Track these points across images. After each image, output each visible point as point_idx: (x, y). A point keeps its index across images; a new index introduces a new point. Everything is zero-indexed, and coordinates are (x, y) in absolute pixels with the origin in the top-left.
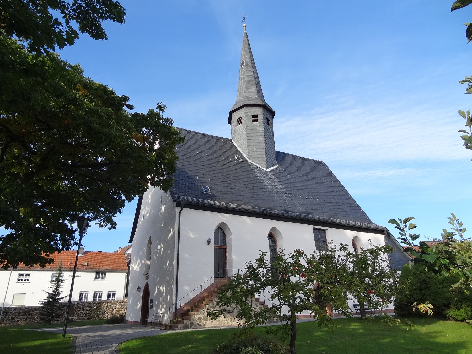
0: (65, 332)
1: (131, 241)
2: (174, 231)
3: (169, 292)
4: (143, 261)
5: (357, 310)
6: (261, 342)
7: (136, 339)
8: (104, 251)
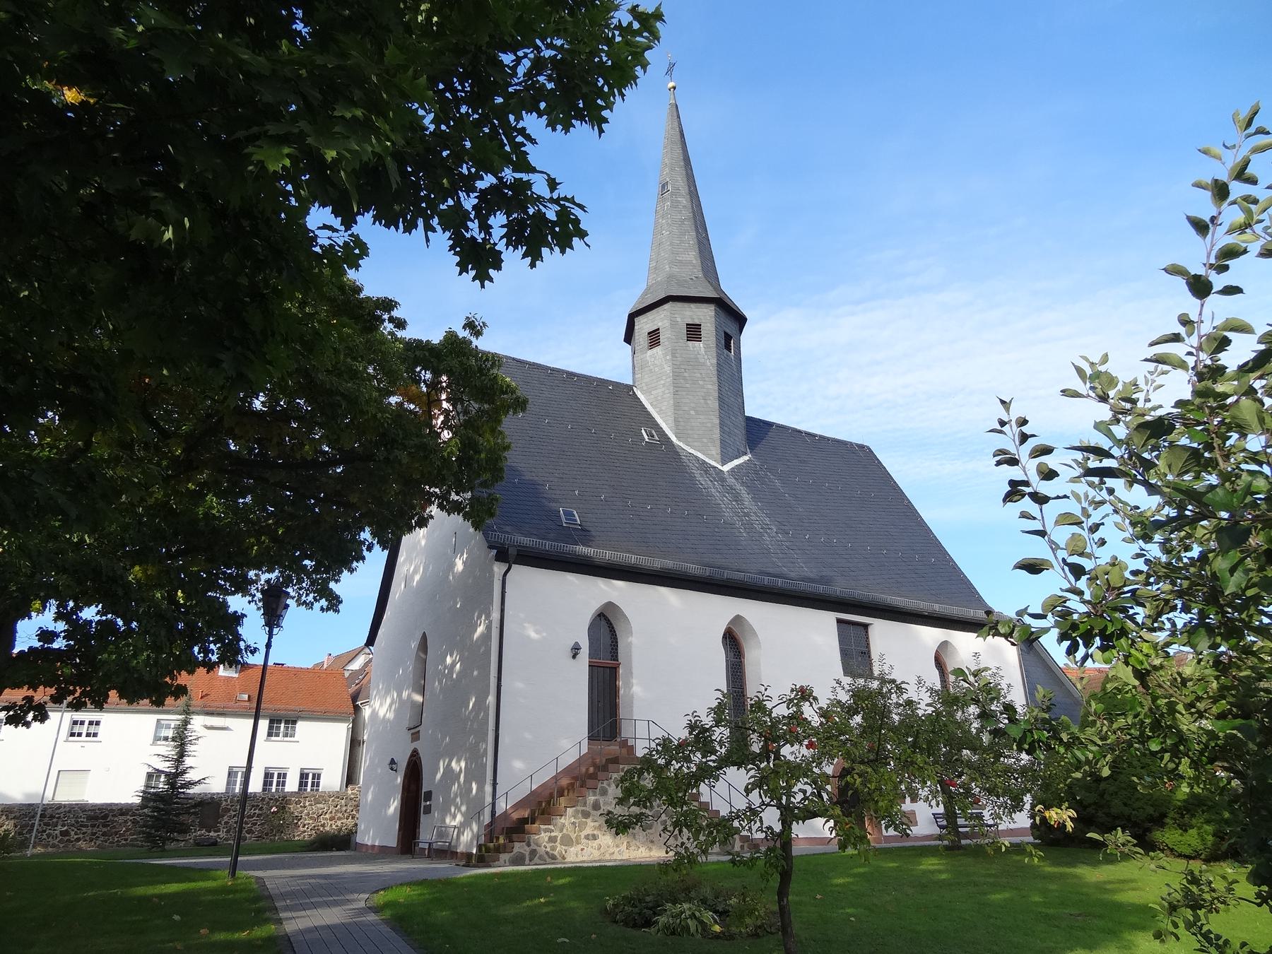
0: (234, 867)
1: (371, 641)
2: (491, 622)
3: (474, 773)
4: (405, 694)
5: (941, 827)
6: (707, 892)
7: (409, 884)
8: (289, 664)
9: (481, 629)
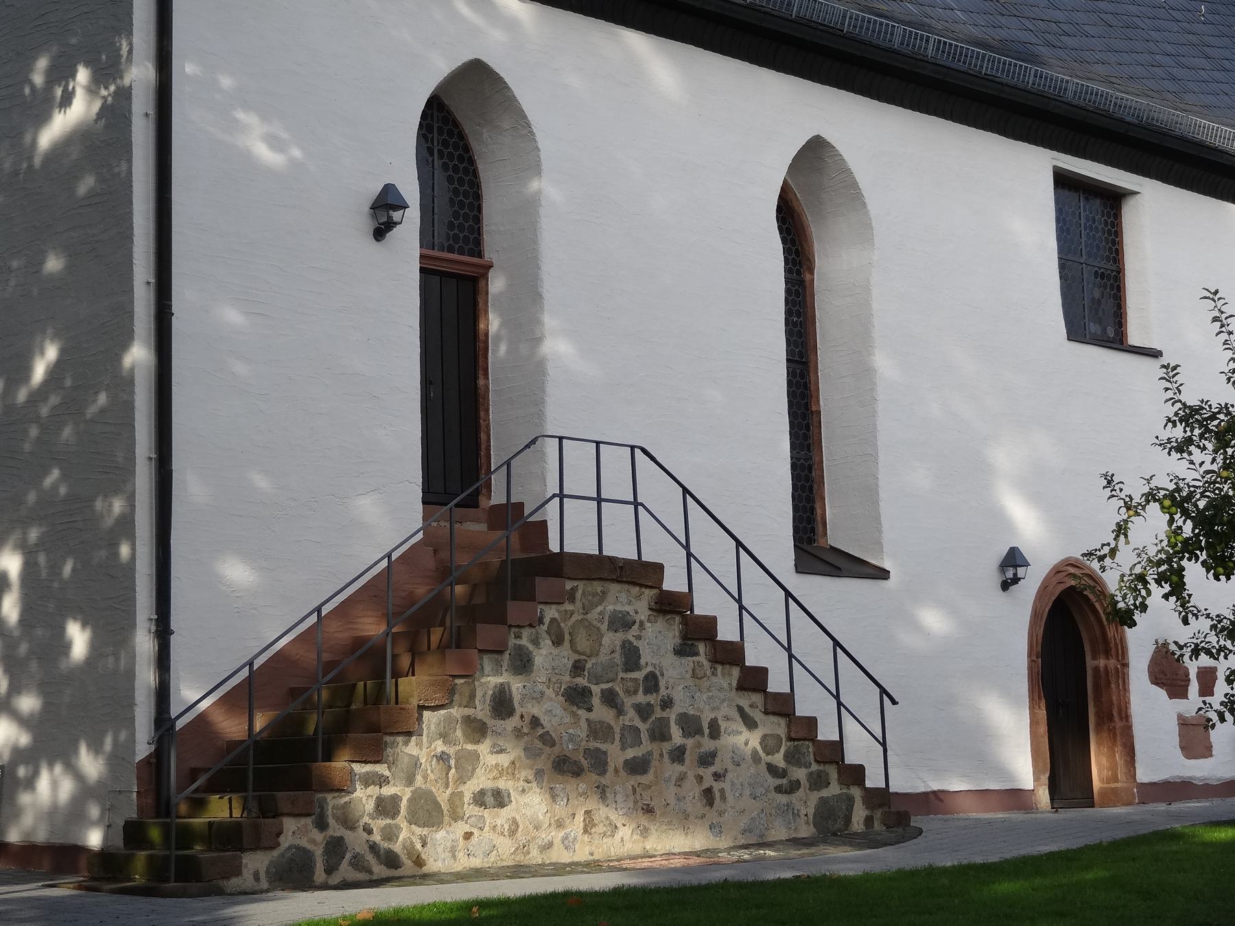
9: (78, 110)
